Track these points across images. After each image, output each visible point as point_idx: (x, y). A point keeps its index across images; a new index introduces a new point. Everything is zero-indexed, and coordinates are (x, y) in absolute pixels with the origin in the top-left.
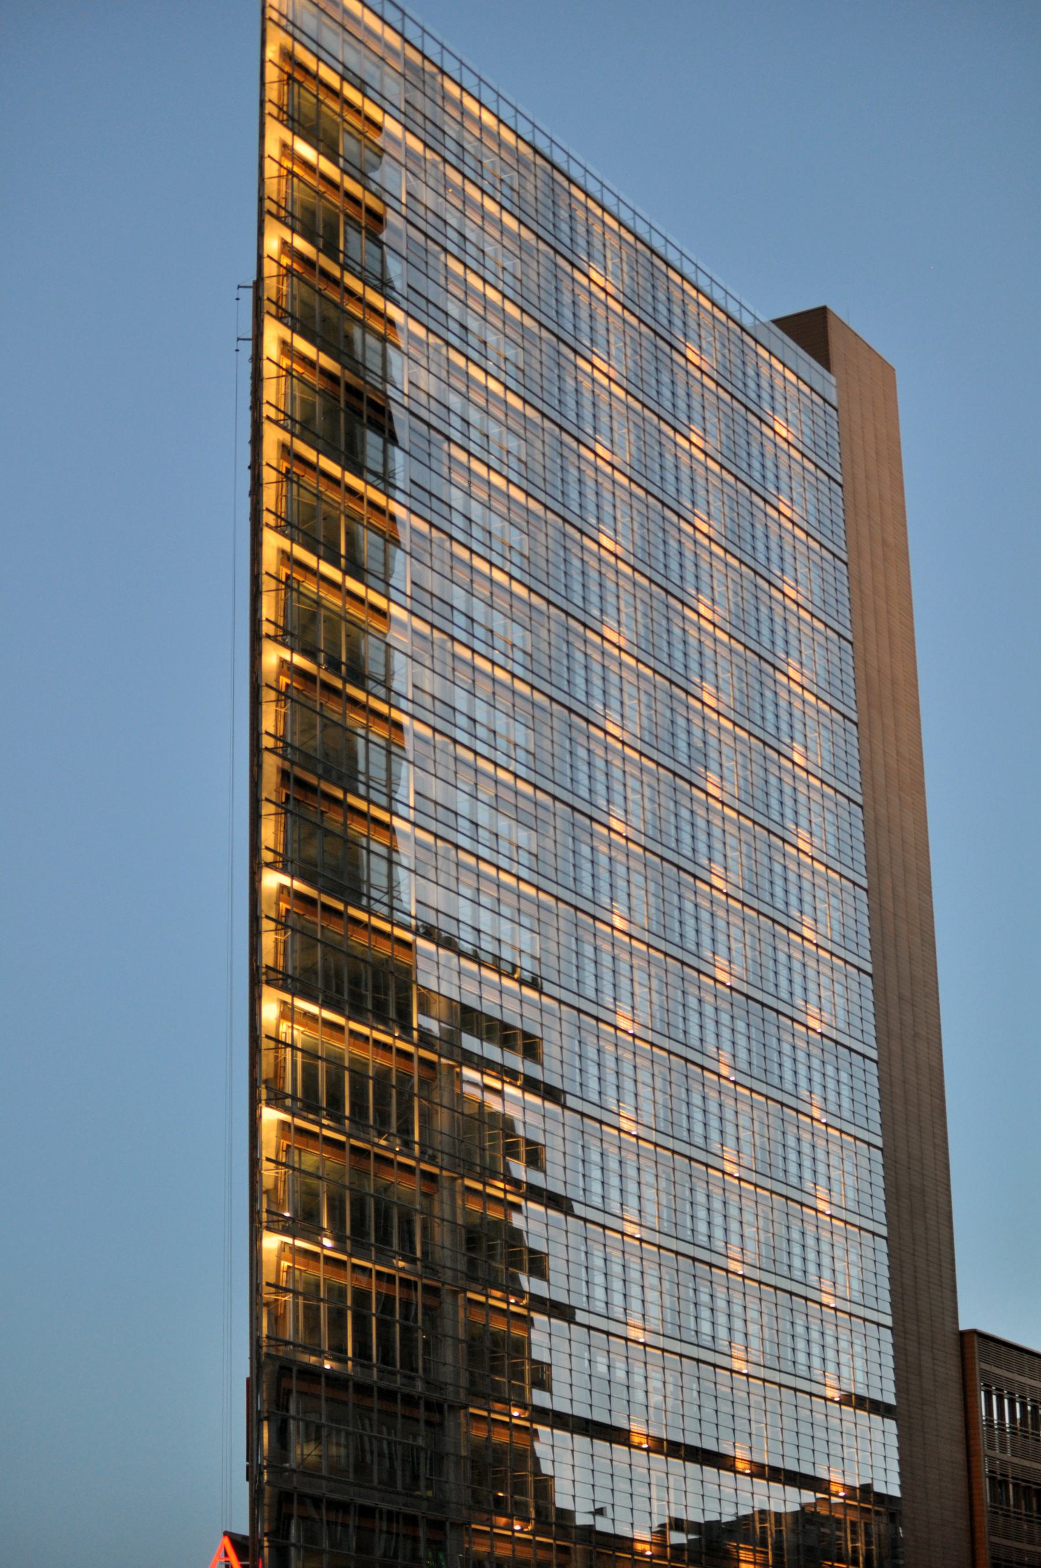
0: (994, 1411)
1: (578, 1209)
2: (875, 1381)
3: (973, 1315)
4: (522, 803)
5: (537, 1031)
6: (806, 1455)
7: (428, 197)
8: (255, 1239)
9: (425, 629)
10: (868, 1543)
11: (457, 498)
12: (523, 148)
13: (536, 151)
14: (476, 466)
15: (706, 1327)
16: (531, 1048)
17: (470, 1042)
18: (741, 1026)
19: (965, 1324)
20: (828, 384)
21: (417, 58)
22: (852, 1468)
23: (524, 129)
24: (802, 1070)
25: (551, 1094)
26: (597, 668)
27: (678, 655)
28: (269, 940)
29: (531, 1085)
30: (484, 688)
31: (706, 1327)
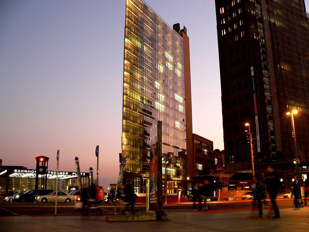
0: (195, 141)
1: (155, 119)
2: (184, 147)
3: (194, 132)
4: (151, 78)
5: (151, 123)
6: (177, 145)
7: (142, 16)
8: (123, 90)
9: (141, 40)
10: (184, 173)
11: (145, 57)
12: (152, 13)
13: (154, 13)
14: (147, 44)
15: (168, 132)
16: (151, 113)
17: (145, 124)
18: (172, 102)
19: (193, 133)
20: (182, 39)
21: (142, 3)
22: (182, 147)
23: (153, 11)
24: (178, 116)
25: (153, 118)
26: (158, 75)
27: (167, 83)
28: (124, 103)
29: (151, 117)
30: (147, 66)
31: (168, 132)
